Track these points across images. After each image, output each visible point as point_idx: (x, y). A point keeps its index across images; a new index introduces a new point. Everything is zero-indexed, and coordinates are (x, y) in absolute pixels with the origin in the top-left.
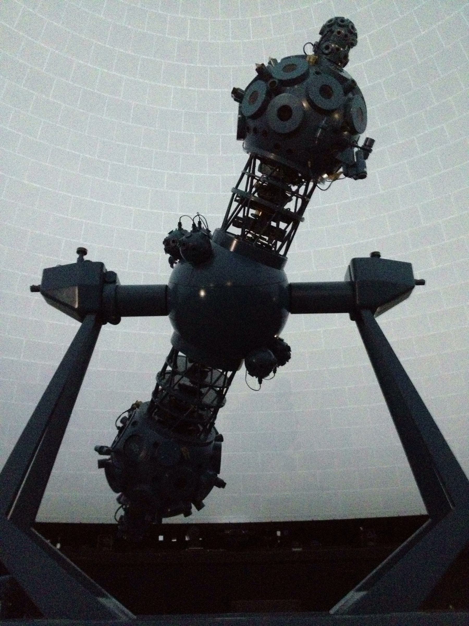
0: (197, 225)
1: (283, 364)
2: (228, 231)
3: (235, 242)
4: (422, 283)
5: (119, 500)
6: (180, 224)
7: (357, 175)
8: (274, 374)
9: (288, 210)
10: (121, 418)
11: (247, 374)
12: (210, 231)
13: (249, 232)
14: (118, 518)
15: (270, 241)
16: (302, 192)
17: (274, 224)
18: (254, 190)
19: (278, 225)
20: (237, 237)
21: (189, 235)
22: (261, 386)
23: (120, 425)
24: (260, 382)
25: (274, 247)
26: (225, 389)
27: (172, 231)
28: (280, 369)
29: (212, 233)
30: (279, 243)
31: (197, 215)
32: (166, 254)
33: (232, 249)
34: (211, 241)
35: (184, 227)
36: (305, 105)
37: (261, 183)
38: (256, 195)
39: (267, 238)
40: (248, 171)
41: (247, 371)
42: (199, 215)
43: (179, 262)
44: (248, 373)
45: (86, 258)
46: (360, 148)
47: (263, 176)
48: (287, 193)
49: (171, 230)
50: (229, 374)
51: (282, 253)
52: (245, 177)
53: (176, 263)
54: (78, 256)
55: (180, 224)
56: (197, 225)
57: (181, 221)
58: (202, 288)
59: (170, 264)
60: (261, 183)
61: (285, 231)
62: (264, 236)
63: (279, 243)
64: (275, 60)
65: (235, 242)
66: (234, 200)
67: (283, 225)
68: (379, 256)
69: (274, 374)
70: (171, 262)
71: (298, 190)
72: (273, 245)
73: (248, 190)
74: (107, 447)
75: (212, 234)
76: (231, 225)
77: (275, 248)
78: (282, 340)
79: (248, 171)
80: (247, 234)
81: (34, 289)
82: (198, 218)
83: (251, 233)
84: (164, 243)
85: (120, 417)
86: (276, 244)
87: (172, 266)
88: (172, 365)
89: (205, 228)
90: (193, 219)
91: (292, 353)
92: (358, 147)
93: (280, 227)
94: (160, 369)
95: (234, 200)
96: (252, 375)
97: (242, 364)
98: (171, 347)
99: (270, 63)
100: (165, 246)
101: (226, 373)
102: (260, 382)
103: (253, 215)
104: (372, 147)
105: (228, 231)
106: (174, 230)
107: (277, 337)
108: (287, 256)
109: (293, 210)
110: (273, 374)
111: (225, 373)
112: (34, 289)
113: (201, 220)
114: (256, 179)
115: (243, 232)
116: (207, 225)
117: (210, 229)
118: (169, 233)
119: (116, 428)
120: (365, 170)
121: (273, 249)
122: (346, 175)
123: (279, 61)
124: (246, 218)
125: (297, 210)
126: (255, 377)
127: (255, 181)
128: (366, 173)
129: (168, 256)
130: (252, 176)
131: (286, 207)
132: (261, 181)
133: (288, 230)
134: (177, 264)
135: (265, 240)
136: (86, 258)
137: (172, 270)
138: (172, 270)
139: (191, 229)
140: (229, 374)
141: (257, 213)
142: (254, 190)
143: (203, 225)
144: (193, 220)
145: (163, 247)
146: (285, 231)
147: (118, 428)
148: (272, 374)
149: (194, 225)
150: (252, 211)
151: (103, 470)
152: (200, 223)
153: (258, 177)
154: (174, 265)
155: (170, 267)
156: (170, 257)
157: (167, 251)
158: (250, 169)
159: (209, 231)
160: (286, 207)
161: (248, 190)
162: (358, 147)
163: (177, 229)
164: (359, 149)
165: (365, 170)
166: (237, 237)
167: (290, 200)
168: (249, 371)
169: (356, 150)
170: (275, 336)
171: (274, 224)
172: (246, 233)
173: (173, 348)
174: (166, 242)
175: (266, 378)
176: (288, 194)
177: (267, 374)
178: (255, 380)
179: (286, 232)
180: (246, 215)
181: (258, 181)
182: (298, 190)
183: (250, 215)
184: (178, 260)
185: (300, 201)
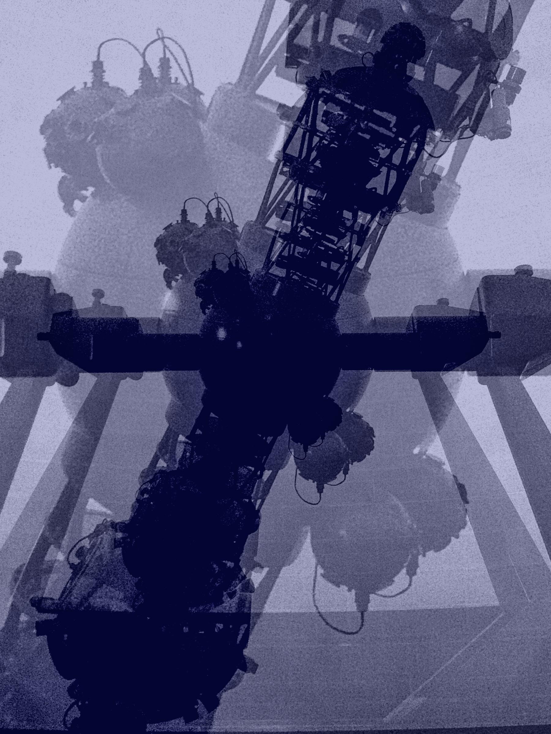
0: (156, 73)
1: (360, 459)
2: (259, 92)
3: (278, 286)
4: (497, 335)
5: (71, 691)
6: (184, 213)
7: (494, 131)
8: (411, 578)
9: (374, 190)
10: (78, 547)
11: (320, 578)
12: (198, 93)
13: (294, 274)
14: (69, 720)
15: (319, 285)
16: (396, 160)
17: (324, 264)
18: (314, 154)
19: (329, 265)
20: (281, 279)
21: (129, 106)
22: (322, 496)
23: (76, 561)
24: (320, 490)
25: (324, 292)
26: (259, 501)
27: (71, 92)
28: (355, 468)
29: (206, 100)
30: (330, 287)
31: (156, 37)
32: (159, 264)
33: (275, 293)
34: (204, 127)
35: (191, 218)
36: (404, 8)
37: (326, 142)
38: (318, 164)
39: (393, 119)
40: (303, 122)
41: (319, 567)
42: (162, 39)
43: (212, 307)
44: (323, 576)
45: (103, 301)
46: (427, 176)
47: (329, 130)
48: (341, 228)
49: (70, 88)
50: (270, 439)
51: (333, 298)
52: (300, 131)
53: (83, 199)
54: (92, 299)
55: (184, 213)
56: (156, 73)
57: (186, 208)
58: (221, 325)
59: (64, 200)
60: (326, 142)
61: (337, 272)
62: (380, 126)
63: (330, 287)
64: (328, 73)
65: (278, 286)
66: (279, 171)
67: (335, 266)
68: (448, 303)
69: (411, 578)
70: (203, 307)
71: (390, 157)
72: (323, 289)
73: (304, 155)
74: (52, 599)
75: (207, 105)
76: (273, 73)
77: (326, 292)
78: (359, 417)
79: (303, 122)
80: (292, 276)
81: (41, 337)
82: (217, 203)
83: (297, 275)
84: (43, 130)
85: (75, 546)
86: (326, 288)
87: (69, 209)
88: (167, 457)
89: (227, 220)
90: (142, 51)
91: (377, 440)
92: (424, 175)
93: (332, 268)
94: (146, 464)
95: (279, 171)
96: (307, 477)
97: (302, 543)
98: (165, 425)
99: (322, 75)
100: (47, 139)
101: (266, 439)
102: (320, 490)
103: (346, 40)
104: (520, 84)
105: (259, 92)
106: (79, 87)
107: (421, 454)
108: (460, 179)
109: (381, 191)
110: (321, 441)
111: (259, 473)
112: (41, 337)
113: (168, 55)
114: (304, 211)
115: (288, 273)
116: (191, 72)
117: (236, 222)
118: (62, 98)
119: (69, 566)
120: (508, 122)
121: (323, 293)
122: (411, 209)
123: (333, 73)
124: (291, 257)
125: (389, 190)
126: (311, 481)
127: (316, 140)
128: (511, 130)
129: (163, 267)
130: (313, 131)
131: (368, 186)
132: (326, 140)
133: (341, 271)
134: (86, 203)
135: (313, 282)
136: (103, 301)
137: (68, 222)
138: (202, 317)
139: (137, 85)
140: (270, 439)
141: (358, 34)
142: (314, 154)
143: (223, 215)
144: (143, 55)
145: (42, 142)
146: (337, 272)
147: (72, 566)
148: (340, 476)
149: (145, 72)
150: (300, 249)
151: (43, 639)
152: (165, 64)
153: (322, 133)
154: (77, 205)
155: (62, 211)
156: (166, 270)
157: (161, 259)
158: (308, 116)
159: (233, 226)
160: (368, 186)
161: (304, 155)
162: (424, 175)
163: (89, 85)
164: (426, 178)
165: (508, 122)
166: (281, 279)
167: (377, 172)
168: (292, 437)
169: (422, 178)
170: (416, 451)
171: (324, 264)
172: (291, 274)
173: (169, 429)
174: (159, 243)
175: (331, 483)
176: (373, 163)
177: (333, 476)
178: (312, 485)
179: (457, 97)
180: (320, 38)
181: (306, 213)
182: (390, 157)
183: (335, 42)
184: (91, 189)
185: (394, 174)
